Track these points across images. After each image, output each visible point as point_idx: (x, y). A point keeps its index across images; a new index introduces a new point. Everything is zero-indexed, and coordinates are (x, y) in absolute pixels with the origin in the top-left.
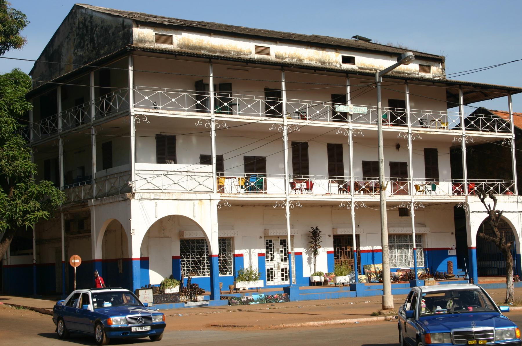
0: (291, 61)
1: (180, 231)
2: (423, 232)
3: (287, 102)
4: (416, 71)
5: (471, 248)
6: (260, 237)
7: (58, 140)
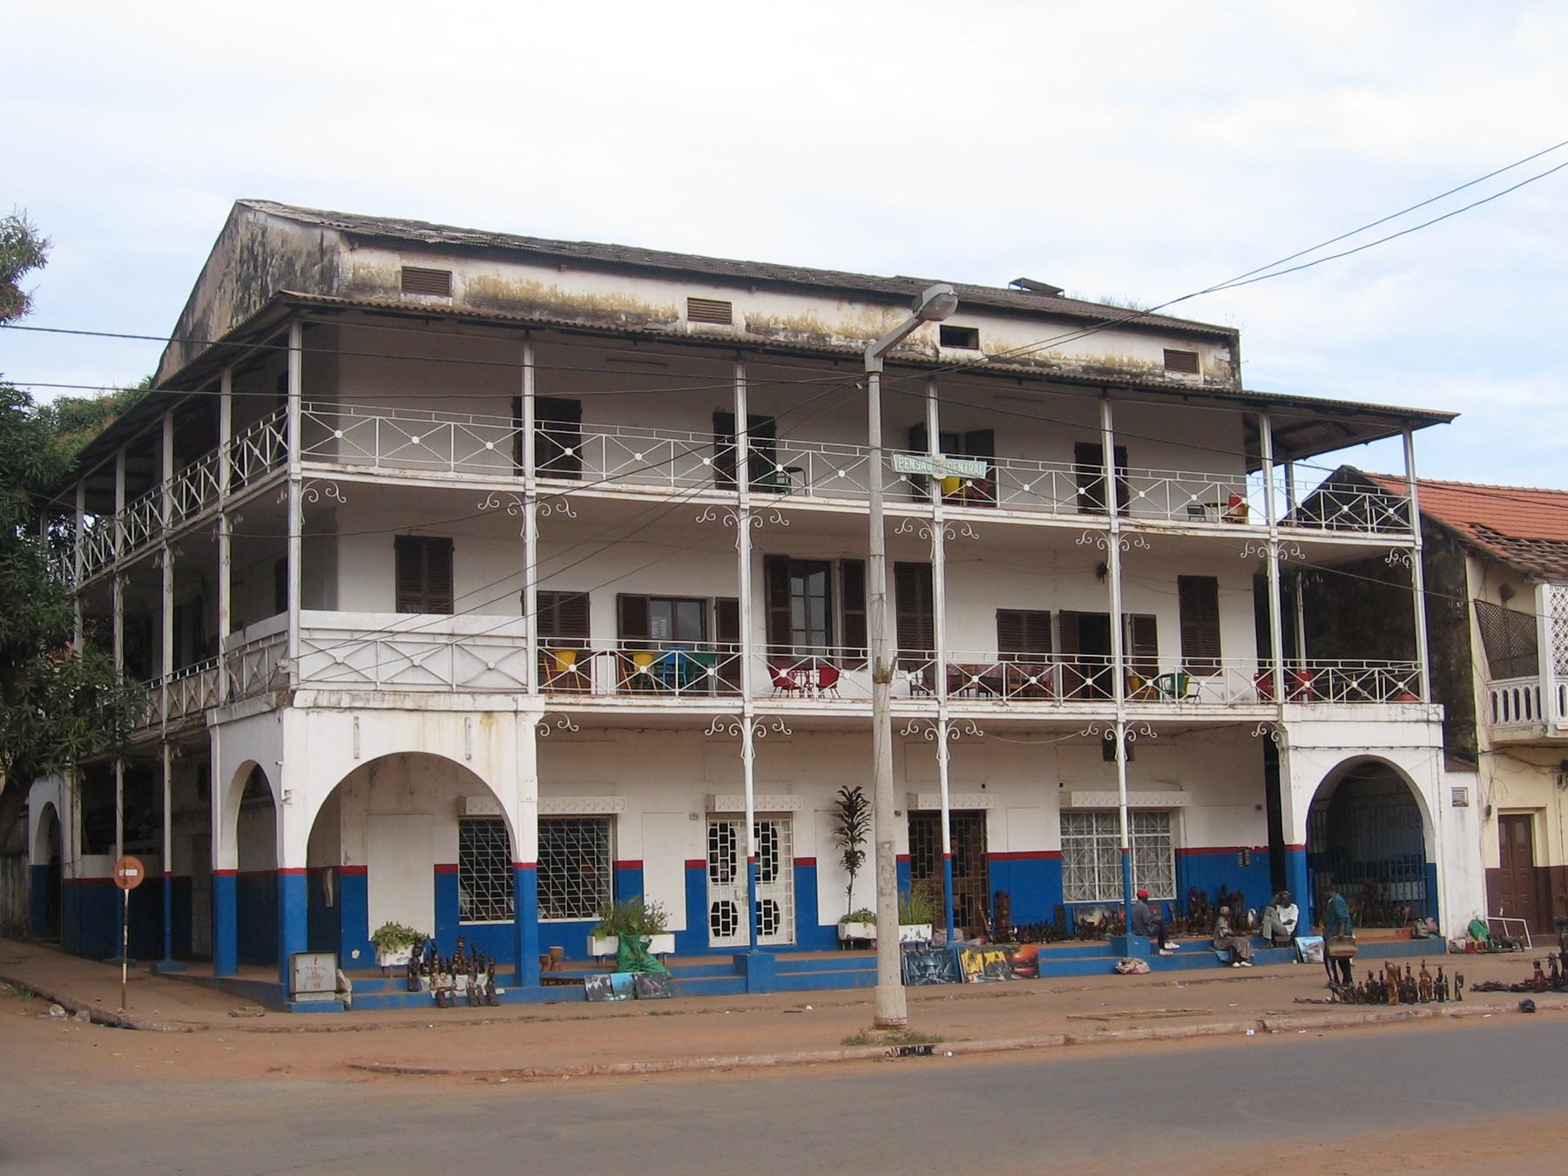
0: (793, 340)
1: (460, 797)
2: (1171, 804)
3: (751, 447)
4: (1155, 366)
5: (515, 868)
6: (694, 817)
7: (162, 551)
